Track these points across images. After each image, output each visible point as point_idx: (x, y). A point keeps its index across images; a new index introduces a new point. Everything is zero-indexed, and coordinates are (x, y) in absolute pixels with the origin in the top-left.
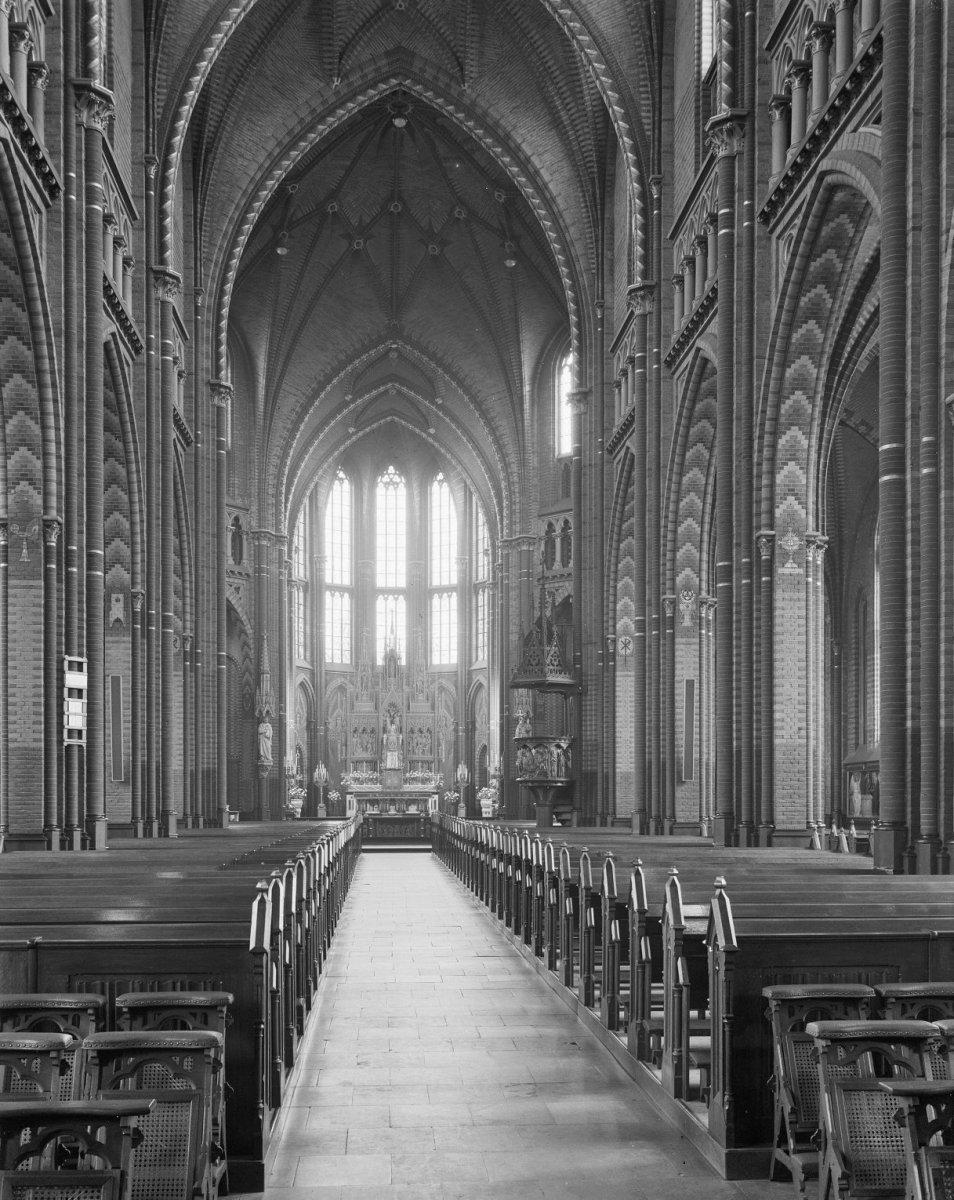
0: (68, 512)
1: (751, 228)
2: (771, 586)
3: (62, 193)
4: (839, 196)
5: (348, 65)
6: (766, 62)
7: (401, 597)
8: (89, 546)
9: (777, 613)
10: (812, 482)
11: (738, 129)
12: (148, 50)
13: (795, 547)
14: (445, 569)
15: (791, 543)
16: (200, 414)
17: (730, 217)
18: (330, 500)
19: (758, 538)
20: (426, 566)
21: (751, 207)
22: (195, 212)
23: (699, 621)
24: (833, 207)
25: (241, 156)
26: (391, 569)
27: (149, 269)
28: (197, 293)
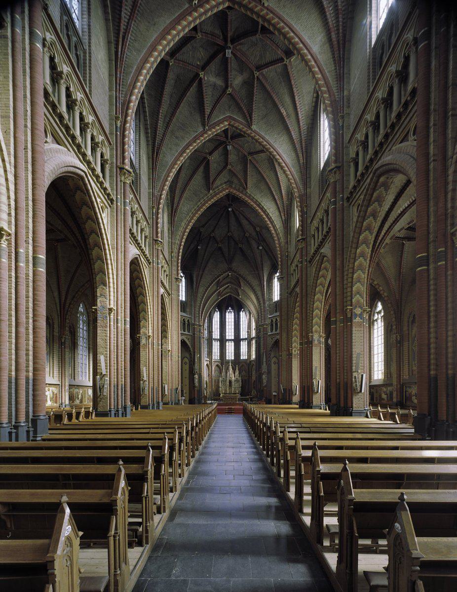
0: (117, 306)
1: (343, 204)
2: (351, 325)
3: (115, 202)
4: (325, 258)
5: (215, 186)
6: (347, 147)
7: (233, 342)
8: (124, 318)
9: (353, 335)
10: (365, 290)
11: (338, 171)
12: (153, 175)
15: (358, 311)
17: (335, 201)
19: (346, 310)
21: (343, 197)
23: (320, 343)
24: (379, 184)
26: (230, 334)
27: (153, 239)
28: (172, 252)
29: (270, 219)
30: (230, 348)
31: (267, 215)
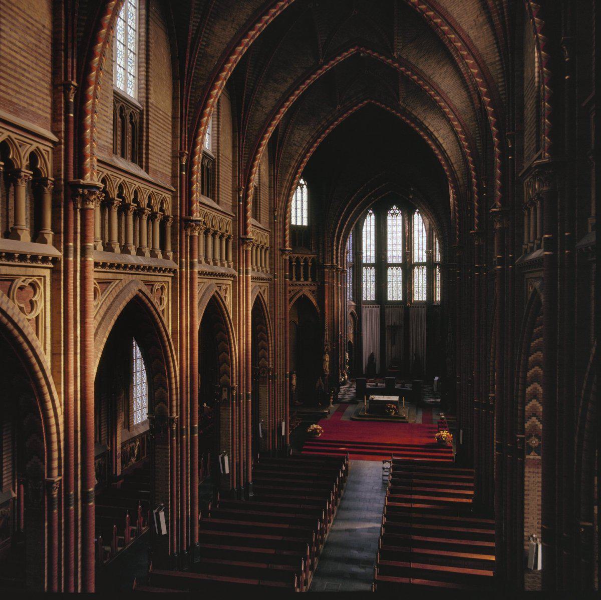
13: (536, 445)
14: (420, 254)
16: (276, 265)
18: (365, 224)
20: (411, 253)
22: (274, 173)
25: (295, 145)
26: (394, 252)
28: (275, 210)
29: (439, 146)
30: (394, 278)
31: (435, 140)
